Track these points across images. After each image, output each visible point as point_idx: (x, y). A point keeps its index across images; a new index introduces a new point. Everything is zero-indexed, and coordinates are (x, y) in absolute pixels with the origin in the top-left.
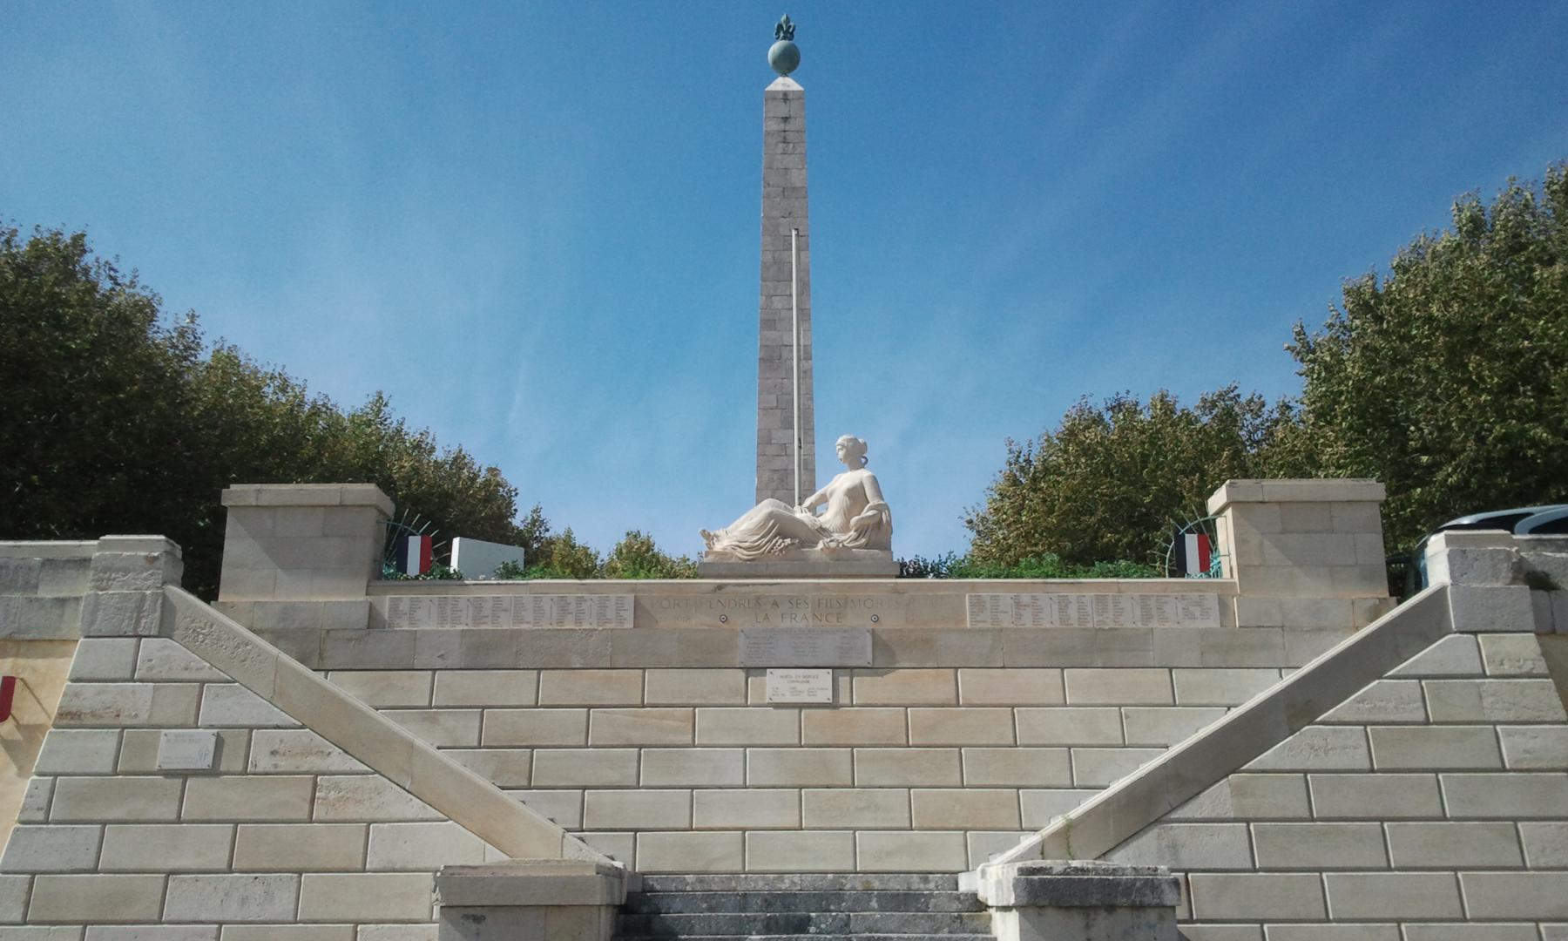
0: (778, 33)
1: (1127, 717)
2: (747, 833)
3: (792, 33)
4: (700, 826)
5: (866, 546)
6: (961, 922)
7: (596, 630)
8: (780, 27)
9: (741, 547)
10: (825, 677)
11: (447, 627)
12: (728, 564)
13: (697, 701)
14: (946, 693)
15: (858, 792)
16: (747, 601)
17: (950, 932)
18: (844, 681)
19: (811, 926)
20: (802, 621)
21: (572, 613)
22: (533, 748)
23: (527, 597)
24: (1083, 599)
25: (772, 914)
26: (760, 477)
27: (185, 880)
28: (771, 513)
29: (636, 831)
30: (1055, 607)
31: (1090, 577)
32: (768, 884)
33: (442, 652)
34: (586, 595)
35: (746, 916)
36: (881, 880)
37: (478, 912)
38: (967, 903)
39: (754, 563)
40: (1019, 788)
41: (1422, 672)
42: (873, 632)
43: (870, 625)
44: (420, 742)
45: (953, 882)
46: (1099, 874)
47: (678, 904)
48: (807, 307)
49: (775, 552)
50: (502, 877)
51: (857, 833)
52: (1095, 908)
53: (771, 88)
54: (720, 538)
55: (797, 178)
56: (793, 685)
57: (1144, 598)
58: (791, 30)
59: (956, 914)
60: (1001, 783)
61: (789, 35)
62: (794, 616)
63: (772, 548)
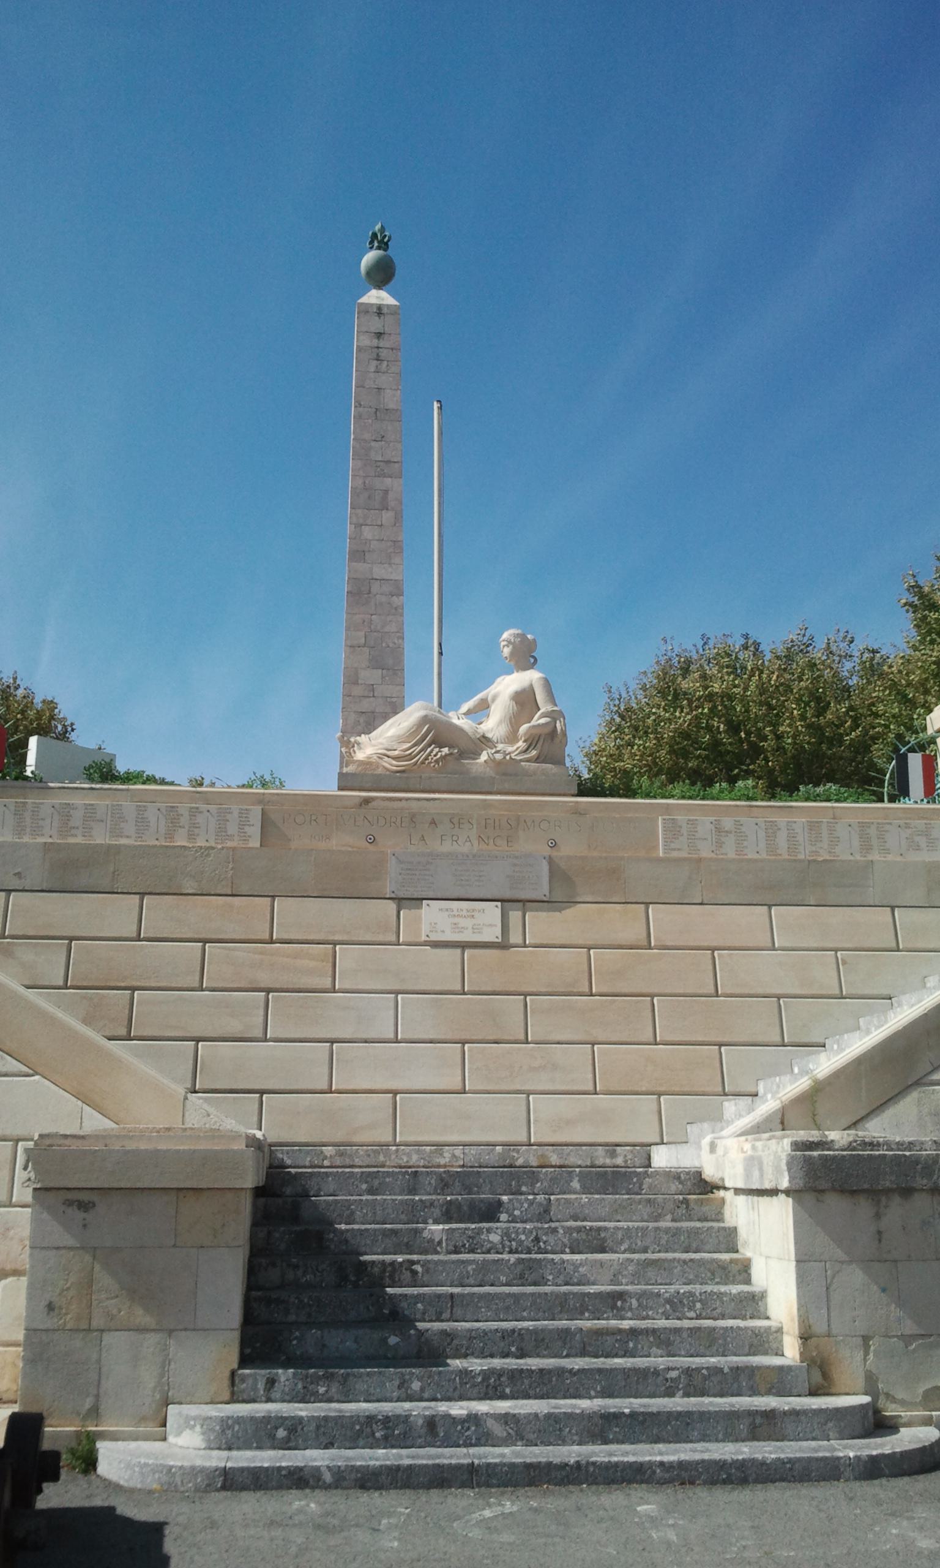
0: (371, 242)
1: (844, 963)
2: (398, 1096)
3: (386, 244)
4: (342, 1087)
5: (537, 760)
6: (687, 1208)
7: (213, 848)
8: (375, 235)
9: (388, 757)
10: (492, 912)
11: (26, 839)
12: (373, 775)
13: (337, 937)
14: (633, 932)
15: (532, 1049)
16: (399, 820)
17: (673, 1220)
18: (515, 916)
19: (502, 1213)
20: (465, 845)
21: (184, 827)
22: (133, 989)
23: (129, 808)
24: (794, 825)
25: (453, 1197)
26: (345, 719)
28: (426, 716)
29: (262, 1092)
30: (762, 834)
31: (796, 801)
32: (424, 1159)
33: (19, 870)
34: (203, 807)
35: (421, 1200)
37: (84, 1197)
38: (689, 1183)
39: (405, 775)
40: (720, 1045)
42: (551, 861)
43: (547, 851)
45: (645, 1155)
46: (892, 1150)
47: (331, 1186)
48: (399, 539)
49: (431, 762)
50: (118, 1150)
51: (531, 1097)
52: (887, 1192)
53: (364, 300)
54: (362, 746)
55: (391, 399)
56: (456, 920)
57: (862, 825)
58: (386, 240)
59: (681, 1197)
60: (700, 1039)
61: (384, 245)
62: (455, 838)
63: (426, 759)
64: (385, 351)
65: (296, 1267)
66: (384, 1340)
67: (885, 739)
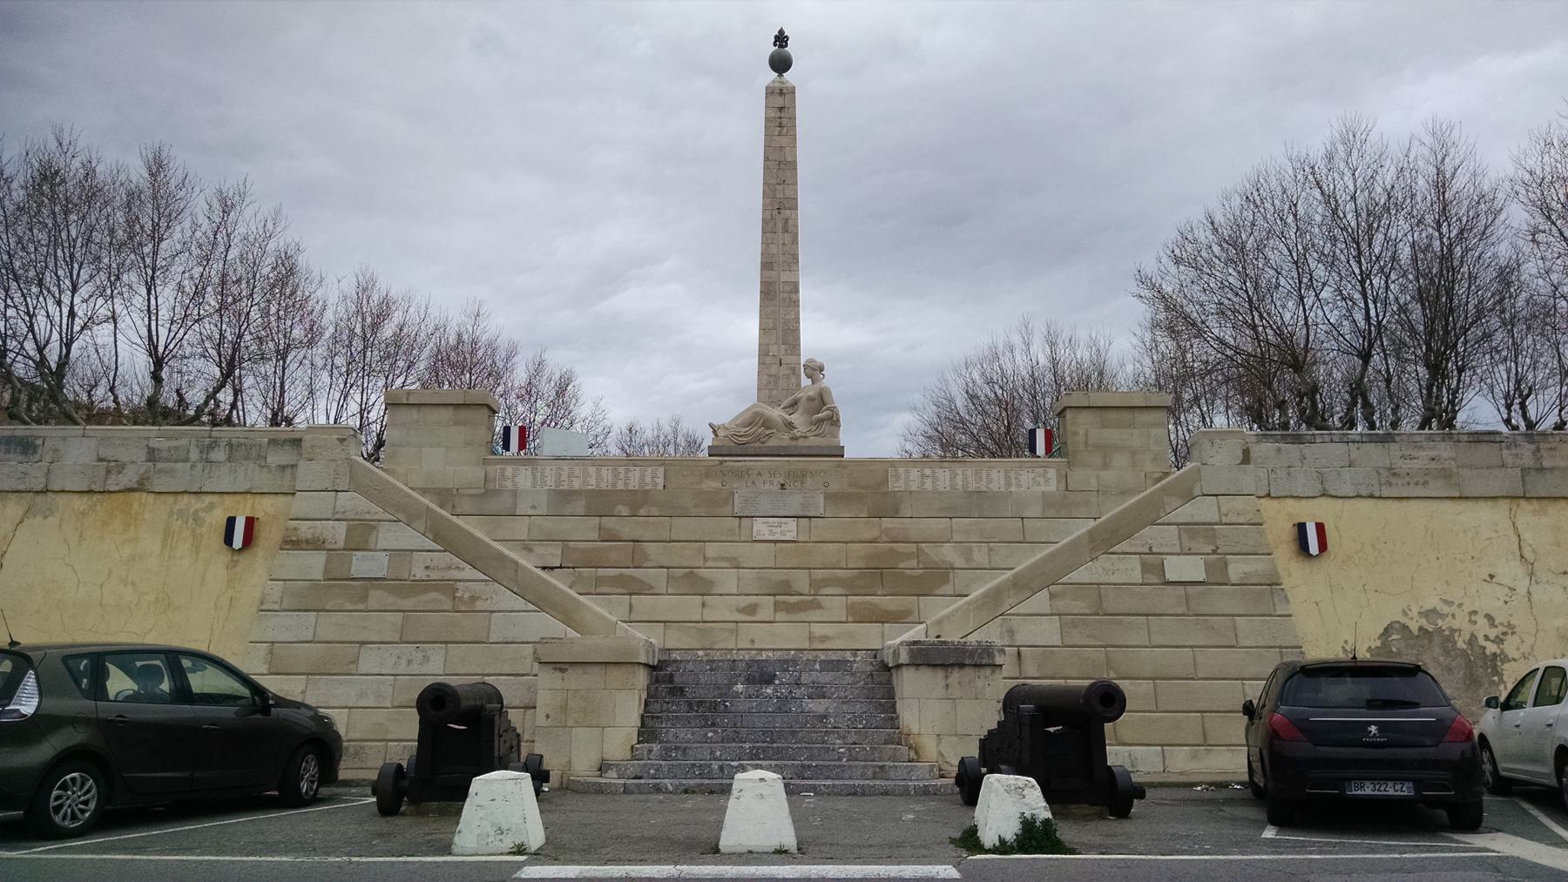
10: (792, 523)
27: (371, 649)
36: (826, 656)
41: (1180, 520)
44: (522, 561)
56: (771, 529)
64: (785, 120)
65: (668, 703)
66: (706, 735)
67: (1428, 297)
